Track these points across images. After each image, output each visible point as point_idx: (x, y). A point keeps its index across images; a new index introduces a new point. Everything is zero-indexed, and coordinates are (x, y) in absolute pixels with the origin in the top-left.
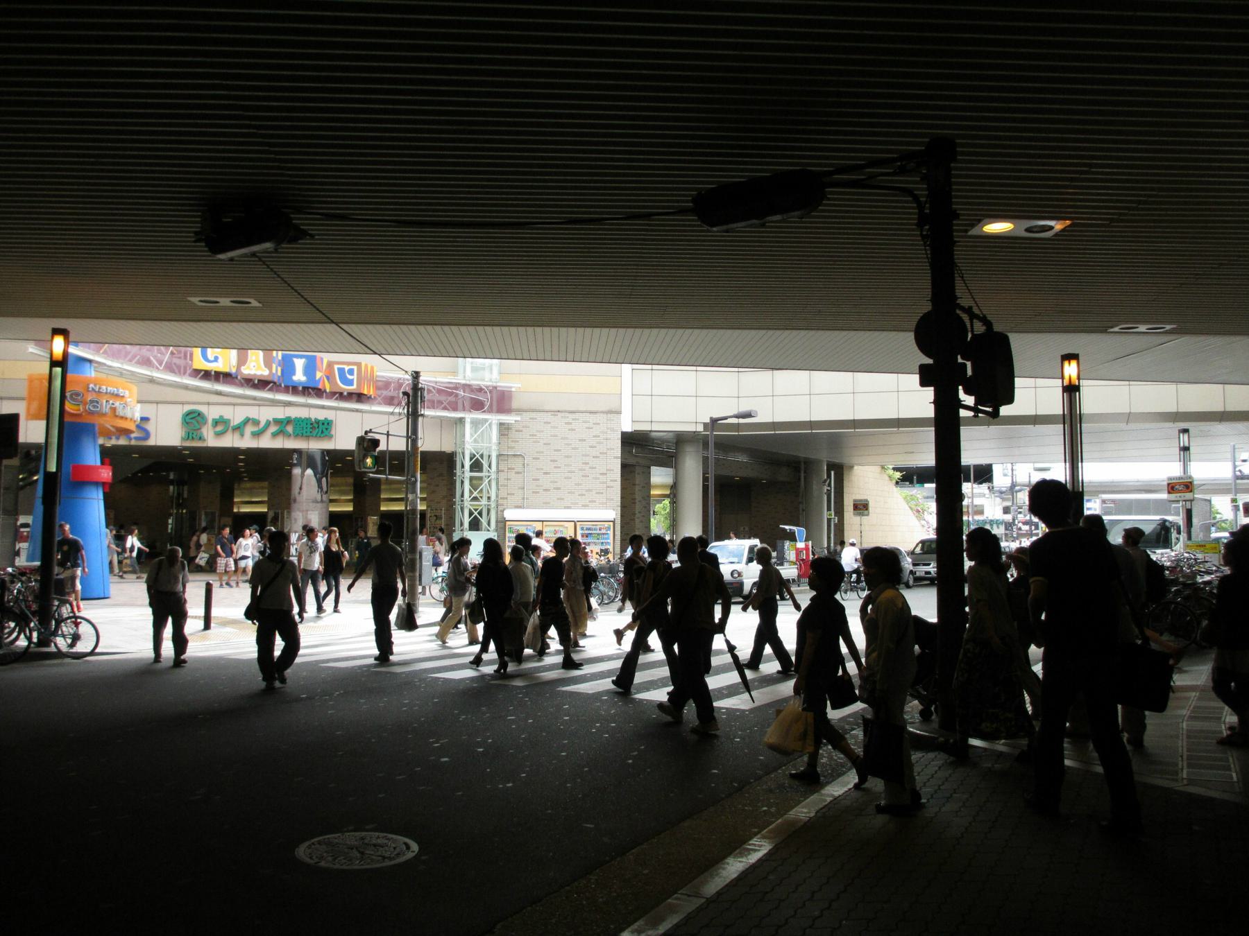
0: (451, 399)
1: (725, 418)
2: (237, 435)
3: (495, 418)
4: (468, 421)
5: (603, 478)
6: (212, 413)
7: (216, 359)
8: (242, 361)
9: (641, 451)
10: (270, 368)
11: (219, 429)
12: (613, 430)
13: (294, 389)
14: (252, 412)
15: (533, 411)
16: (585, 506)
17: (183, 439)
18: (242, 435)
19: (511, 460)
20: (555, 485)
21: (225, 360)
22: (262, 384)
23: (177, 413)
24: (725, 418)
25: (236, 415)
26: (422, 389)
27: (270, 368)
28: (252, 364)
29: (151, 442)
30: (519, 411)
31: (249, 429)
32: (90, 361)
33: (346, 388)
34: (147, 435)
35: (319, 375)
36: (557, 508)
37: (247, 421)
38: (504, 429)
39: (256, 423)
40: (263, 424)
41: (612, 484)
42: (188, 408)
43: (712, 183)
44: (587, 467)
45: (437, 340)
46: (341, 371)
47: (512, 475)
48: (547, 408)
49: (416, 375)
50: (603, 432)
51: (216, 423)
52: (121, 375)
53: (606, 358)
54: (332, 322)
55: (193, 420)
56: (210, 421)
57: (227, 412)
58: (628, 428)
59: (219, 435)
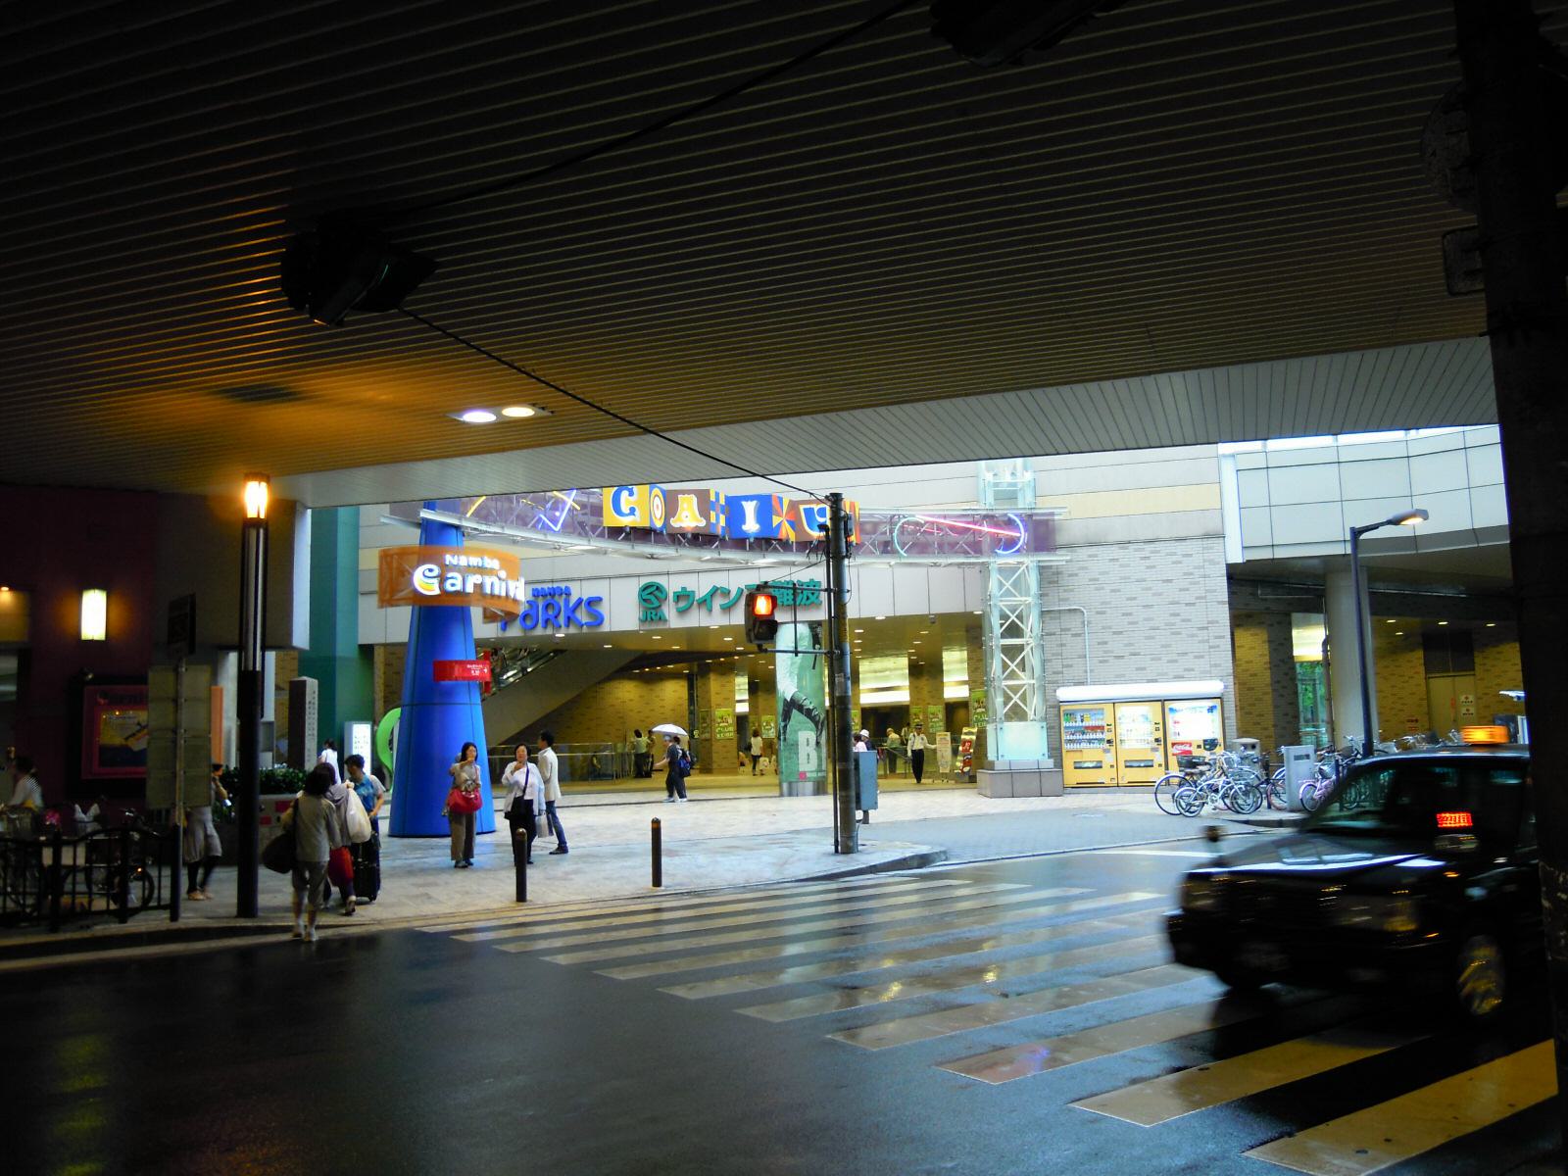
0: (969, 537)
1: (1375, 527)
2: (703, 612)
3: (1030, 561)
4: (993, 567)
5: (1203, 634)
6: (672, 585)
7: (632, 511)
8: (671, 505)
9: (1268, 593)
10: (707, 518)
11: (682, 604)
12: (1212, 562)
13: (740, 543)
14: (720, 580)
15: (1092, 545)
16: (1178, 678)
17: (643, 621)
18: (710, 611)
19: (1065, 617)
20: (1131, 649)
21: (640, 506)
22: (700, 539)
23: (633, 587)
24: (1375, 527)
25: (701, 586)
26: (847, 518)
27: (707, 518)
28: (684, 514)
29: (606, 628)
30: (1069, 546)
31: (718, 602)
32: (457, 528)
33: (626, 521)
34: (599, 620)
35: (776, 520)
36: (1136, 681)
37: (715, 591)
38: (1049, 578)
39: (726, 593)
40: (733, 594)
41: (1217, 642)
42: (644, 581)
43: (426, 290)
44: (1177, 620)
45: (864, 439)
46: (809, 513)
47: (1067, 638)
48: (1111, 539)
49: (835, 499)
50: (1198, 567)
51: (678, 597)
52: (515, 542)
53: (1178, 438)
54: (647, 431)
55: (651, 596)
56: (671, 596)
57: (690, 583)
58: (1237, 557)
59: (682, 612)
